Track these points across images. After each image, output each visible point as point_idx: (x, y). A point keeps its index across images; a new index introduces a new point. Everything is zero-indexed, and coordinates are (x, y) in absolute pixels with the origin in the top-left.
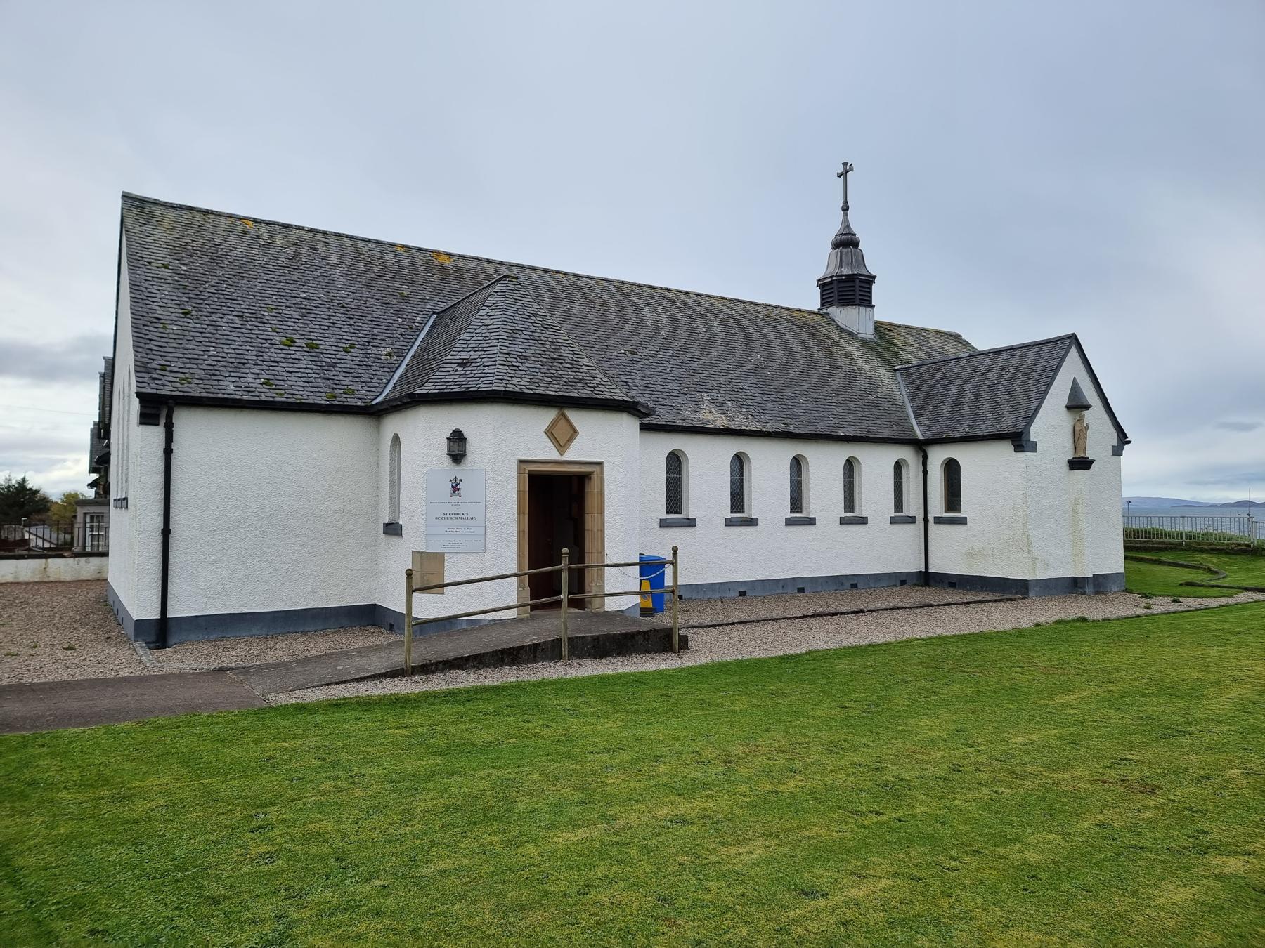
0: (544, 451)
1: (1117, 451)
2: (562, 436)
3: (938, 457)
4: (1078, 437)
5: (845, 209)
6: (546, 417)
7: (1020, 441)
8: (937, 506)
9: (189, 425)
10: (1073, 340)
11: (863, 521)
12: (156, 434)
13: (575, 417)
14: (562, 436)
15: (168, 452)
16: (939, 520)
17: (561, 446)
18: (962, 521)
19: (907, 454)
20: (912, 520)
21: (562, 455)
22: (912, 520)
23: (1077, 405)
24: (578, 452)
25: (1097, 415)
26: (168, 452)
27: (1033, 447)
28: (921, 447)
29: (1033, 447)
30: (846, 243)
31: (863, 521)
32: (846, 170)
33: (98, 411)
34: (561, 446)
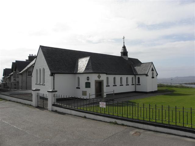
0: (98, 79)
1: (157, 76)
2: (99, 77)
3: (137, 76)
4: (153, 74)
5: (124, 43)
6: (97, 75)
7: (147, 75)
8: (137, 83)
9: (56, 76)
10: (152, 63)
11: (128, 85)
12: (53, 77)
13: (100, 74)
14: (99, 77)
15: (54, 79)
16: (137, 85)
18: (140, 85)
19: (133, 76)
20: (134, 85)
21: (99, 79)
22: (134, 85)
23: (153, 70)
24: (101, 79)
25: (154, 72)
26: (54, 79)
27: (148, 76)
28: (135, 75)
29: (148, 76)
30: (124, 47)
31: (128, 85)
32: (124, 38)
33: (154, 91)
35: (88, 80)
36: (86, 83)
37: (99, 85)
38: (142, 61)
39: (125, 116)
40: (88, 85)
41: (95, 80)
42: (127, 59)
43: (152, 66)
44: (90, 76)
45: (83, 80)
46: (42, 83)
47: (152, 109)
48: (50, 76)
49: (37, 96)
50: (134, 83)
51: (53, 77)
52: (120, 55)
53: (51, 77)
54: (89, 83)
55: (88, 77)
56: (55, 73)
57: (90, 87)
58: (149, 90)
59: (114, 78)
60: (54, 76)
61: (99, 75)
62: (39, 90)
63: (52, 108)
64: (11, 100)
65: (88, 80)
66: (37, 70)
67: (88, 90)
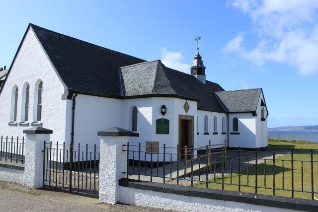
0: (183, 113)
3: (232, 117)
6: (183, 102)
8: (231, 130)
12: (71, 101)
14: (186, 108)
15: (74, 108)
16: (231, 133)
17: (187, 112)
18: (239, 134)
21: (187, 113)
24: (190, 113)
26: (74, 108)
34: (187, 112)
35: (163, 113)
36: (159, 122)
37: (186, 125)
38: (226, 88)
39: (53, 184)
40: (162, 126)
41: (180, 116)
42: (204, 82)
43: (261, 97)
44: (169, 102)
45: (148, 113)
46: (18, 121)
47: (232, 183)
48: (63, 99)
49: (44, 151)
50: (226, 131)
51: (71, 101)
52: (188, 72)
53: (65, 102)
54: (167, 121)
55: (164, 107)
56: (77, 93)
57: (167, 132)
58: (258, 145)
59: (206, 118)
60: (74, 100)
61: (187, 103)
62: (50, 132)
63: (118, 194)
64: (298, 146)
65: (163, 113)
66: (17, 90)
67: (161, 139)
